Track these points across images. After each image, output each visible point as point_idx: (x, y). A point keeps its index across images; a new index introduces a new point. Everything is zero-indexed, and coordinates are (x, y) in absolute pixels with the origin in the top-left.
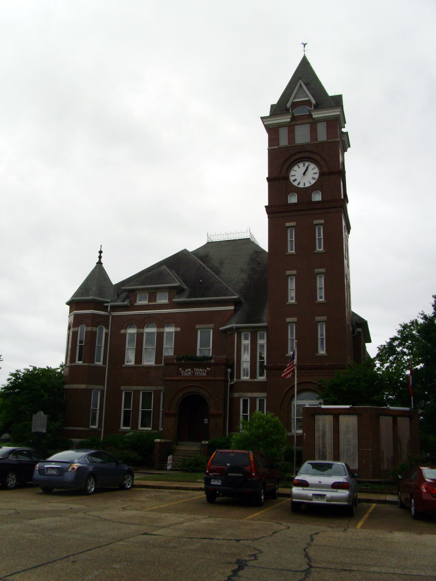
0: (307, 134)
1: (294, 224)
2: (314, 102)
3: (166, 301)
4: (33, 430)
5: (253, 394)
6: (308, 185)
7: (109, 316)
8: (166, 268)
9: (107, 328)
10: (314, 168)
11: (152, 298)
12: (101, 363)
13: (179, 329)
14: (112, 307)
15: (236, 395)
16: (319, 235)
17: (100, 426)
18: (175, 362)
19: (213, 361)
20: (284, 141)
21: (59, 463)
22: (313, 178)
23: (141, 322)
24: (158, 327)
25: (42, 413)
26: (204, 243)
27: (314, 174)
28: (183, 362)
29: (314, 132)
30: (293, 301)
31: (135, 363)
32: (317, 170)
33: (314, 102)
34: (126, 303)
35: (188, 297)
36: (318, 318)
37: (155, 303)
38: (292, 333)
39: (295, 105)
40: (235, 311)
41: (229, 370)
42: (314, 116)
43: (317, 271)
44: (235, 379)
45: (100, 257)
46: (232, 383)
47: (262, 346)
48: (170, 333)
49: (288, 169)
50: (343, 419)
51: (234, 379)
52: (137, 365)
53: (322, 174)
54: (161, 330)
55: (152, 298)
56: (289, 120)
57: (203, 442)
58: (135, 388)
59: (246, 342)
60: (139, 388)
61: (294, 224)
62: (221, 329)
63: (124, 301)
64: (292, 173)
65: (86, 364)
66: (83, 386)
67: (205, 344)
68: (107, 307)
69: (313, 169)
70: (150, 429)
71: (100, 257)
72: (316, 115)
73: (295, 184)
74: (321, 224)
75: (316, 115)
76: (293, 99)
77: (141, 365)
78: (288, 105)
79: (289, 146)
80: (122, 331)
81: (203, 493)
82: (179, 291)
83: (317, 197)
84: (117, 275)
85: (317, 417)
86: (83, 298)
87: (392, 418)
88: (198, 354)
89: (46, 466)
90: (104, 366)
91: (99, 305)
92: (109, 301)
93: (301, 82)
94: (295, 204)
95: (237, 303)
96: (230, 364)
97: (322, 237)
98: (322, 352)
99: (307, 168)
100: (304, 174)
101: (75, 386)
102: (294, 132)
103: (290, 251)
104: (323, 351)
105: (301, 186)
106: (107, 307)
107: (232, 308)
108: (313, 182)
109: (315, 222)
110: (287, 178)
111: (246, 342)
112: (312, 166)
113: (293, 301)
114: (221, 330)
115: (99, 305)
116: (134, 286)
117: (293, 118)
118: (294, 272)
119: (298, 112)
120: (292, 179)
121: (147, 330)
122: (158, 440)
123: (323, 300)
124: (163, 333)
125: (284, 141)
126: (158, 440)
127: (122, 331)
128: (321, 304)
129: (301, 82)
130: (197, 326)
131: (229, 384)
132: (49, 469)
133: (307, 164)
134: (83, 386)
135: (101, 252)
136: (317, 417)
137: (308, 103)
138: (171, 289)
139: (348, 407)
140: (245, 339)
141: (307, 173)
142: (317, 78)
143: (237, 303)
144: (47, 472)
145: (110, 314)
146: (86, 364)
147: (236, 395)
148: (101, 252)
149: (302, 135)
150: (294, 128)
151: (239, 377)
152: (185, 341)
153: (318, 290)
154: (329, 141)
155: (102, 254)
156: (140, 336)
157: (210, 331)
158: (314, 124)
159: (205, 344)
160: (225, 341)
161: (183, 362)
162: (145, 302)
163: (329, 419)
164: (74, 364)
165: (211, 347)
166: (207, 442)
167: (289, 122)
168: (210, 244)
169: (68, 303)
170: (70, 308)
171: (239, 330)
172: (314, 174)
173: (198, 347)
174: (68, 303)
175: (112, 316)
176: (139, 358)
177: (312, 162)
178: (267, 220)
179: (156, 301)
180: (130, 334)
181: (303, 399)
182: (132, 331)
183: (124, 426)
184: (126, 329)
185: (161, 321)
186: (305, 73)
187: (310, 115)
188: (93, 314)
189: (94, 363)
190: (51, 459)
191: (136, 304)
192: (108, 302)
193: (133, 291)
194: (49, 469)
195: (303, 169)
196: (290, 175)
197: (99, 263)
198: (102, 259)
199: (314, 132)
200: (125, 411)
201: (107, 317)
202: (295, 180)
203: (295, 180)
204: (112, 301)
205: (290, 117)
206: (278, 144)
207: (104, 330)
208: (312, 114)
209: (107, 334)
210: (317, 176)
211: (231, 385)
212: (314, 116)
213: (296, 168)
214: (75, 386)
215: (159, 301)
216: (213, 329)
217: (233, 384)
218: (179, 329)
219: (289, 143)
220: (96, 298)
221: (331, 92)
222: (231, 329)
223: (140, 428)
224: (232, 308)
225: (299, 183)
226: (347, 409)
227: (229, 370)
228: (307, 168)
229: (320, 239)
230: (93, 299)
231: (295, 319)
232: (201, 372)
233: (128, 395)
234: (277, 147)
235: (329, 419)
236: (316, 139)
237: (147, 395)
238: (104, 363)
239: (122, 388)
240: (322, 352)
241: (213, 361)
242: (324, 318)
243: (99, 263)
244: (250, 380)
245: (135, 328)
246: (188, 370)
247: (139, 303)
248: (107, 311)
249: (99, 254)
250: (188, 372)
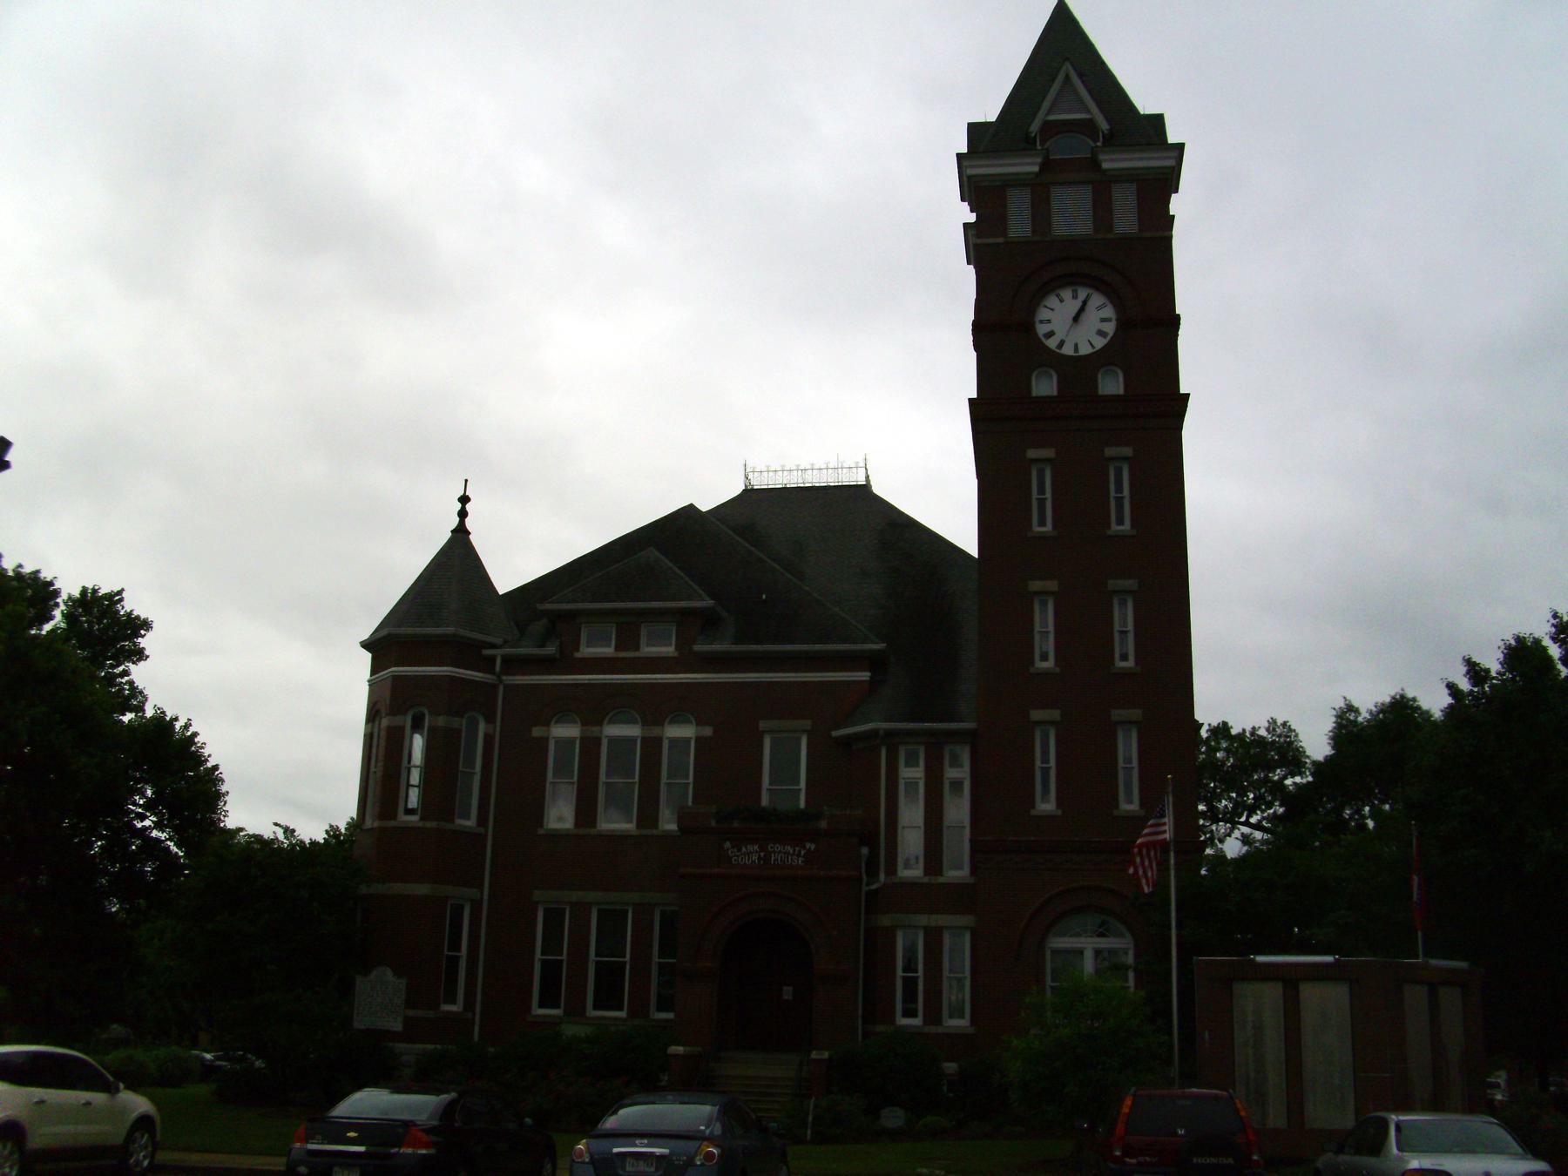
0: (1069, 208)
1: (1049, 453)
2: (1104, 126)
3: (669, 650)
4: (358, 1024)
5: (934, 917)
6: (1085, 350)
7: (494, 687)
8: (657, 554)
9: (490, 720)
11: (628, 639)
12: (470, 823)
13: (708, 731)
14: (506, 660)
15: (885, 921)
16: (1119, 489)
17: (469, 1005)
18: (713, 824)
19: (823, 824)
20: (1019, 226)
21: (661, 1141)
22: (1101, 333)
23: (595, 707)
24: (645, 723)
25: (389, 972)
26: (736, 489)
27: (1103, 320)
28: (736, 824)
29: (1102, 209)
30: (1049, 664)
31: (577, 824)
32: (1109, 312)
33: (1104, 126)
34: (551, 650)
35: (737, 641)
36: (1117, 714)
37: (636, 654)
38: (1045, 752)
39: (1050, 129)
40: (873, 684)
41: (865, 851)
42: (1105, 166)
43: (1113, 584)
44: (882, 877)
45: (463, 514)
46: (874, 887)
47: (957, 785)
48: (567, 743)
50: (1311, 994)
51: (877, 875)
52: (583, 831)
53: (1124, 324)
54: (656, 731)
55: (628, 639)
56: (1036, 169)
57: (814, 1055)
58: (575, 896)
59: (912, 774)
60: (591, 896)
61: (1049, 453)
62: (834, 734)
63: (543, 646)
64: (1043, 314)
65: (429, 824)
66: (422, 889)
67: (786, 772)
68: (493, 659)
69: (1099, 308)
70: (623, 1014)
71: (463, 514)
72: (1110, 162)
73: (1052, 343)
74: (1125, 459)
76: (1049, 112)
77: (593, 831)
78: (1035, 127)
79: (1036, 238)
80: (537, 732)
82: (708, 623)
83: (1111, 385)
84: (512, 565)
85: (1238, 987)
86: (419, 630)
87: (1280, 985)
88: (765, 801)
89: (615, 1150)
90: (481, 830)
91: (466, 651)
92: (499, 641)
95: (875, 663)
96: (875, 837)
97: (1048, 495)
98: (1047, 806)
99: (1085, 303)
100: (1076, 319)
101: (397, 888)
102: (1047, 201)
103: (1115, 528)
104: (1130, 802)
105: (1068, 350)
106: (493, 659)
107: (865, 676)
108: (1100, 343)
109: (1110, 452)
110: (1028, 327)
111: (912, 774)
112: (1097, 299)
113: (1130, 664)
114: (837, 738)
115: (466, 651)
116: (574, 601)
117: (1046, 165)
118: (1053, 585)
120: (1041, 330)
121: (674, 731)
122: (680, 1049)
123: (1130, 664)
124: (659, 740)
125: (1019, 226)
126: (680, 1049)
127: (537, 732)
128: (1126, 675)
130: (763, 725)
131: (865, 889)
132: (629, 1160)
133: (1083, 293)
134: (422, 889)
135: (464, 500)
136: (1238, 987)
137: (1088, 127)
138: (683, 616)
139: (1329, 959)
140: (908, 765)
141: (1083, 317)
142: (1103, 63)
143: (875, 663)
144: (624, 1168)
145: (501, 681)
146: (429, 824)
147: (885, 921)
148: (464, 500)
149: (1072, 214)
151: (891, 870)
152: (727, 762)
153: (1117, 636)
154: (1148, 235)
155: (468, 507)
156: (590, 746)
157: (799, 739)
158: (1103, 185)
159: (786, 772)
160: (851, 770)
161: (736, 824)
162: (608, 651)
163: (1271, 993)
164: (392, 823)
165: (637, 779)
166: (826, 1055)
167: (1037, 175)
168: (750, 496)
169: (366, 645)
170: (373, 659)
171: (892, 740)
172: (1103, 320)
173: (603, 778)
174: (366, 645)
175: (506, 686)
176: (586, 811)
177: (1097, 289)
178: (1184, 433)
179: (637, 648)
180: (558, 741)
181: (1078, 935)
182: (566, 731)
183: (542, 1005)
184: (547, 724)
185: (655, 706)
186: (1064, 50)
187: (1094, 163)
188: (452, 679)
189: (452, 821)
190: (611, 1122)
191: (578, 655)
192: (493, 646)
193: (572, 616)
194: (629, 1160)
195: (1072, 306)
196: (1037, 320)
197: (461, 532)
198: (467, 521)
199: (1102, 209)
200: (544, 963)
201: (494, 687)
202: (1050, 334)
203: (1050, 334)
204: (506, 642)
205: (1039, 160)
206: (1005, 234)
207: (482, 726)
208: (1101, 157)
209: (489, 740)
210: (1110, 328)
211: (868, 893)
212: (1105, 166)
213: (1052, 301)
214: (397, 888)
215: (649, 650)
216: (810, 734)
217: (877, 891)
218: (708, 731)
219: (1034, 232)
220: (462, 632)
221: (1145, 105)
222: (873, 734)
223: (592, 1013)
224: (865, 676)
226: (1327, 965)
227: (865, 851)
228: (1085, 303)
229: (1119, 500)
230: (454, 635)
231: (1055, 714)
232: (788, 855)
233: (554, 918)
234: (1001, 240)
235: (1271, 993)
236: (1110, 228)
237: (612, 920)
238: (482, 820)
239: (538, 895)
240: (1047, 806)
241: (823, 824)
242: (1135, 714)
243: (461, 532)
244: (926, 880)
245: (574, 722)
246: (750, 848)
247: (587, 651)
248: (493, 673)
250: (749, 855)
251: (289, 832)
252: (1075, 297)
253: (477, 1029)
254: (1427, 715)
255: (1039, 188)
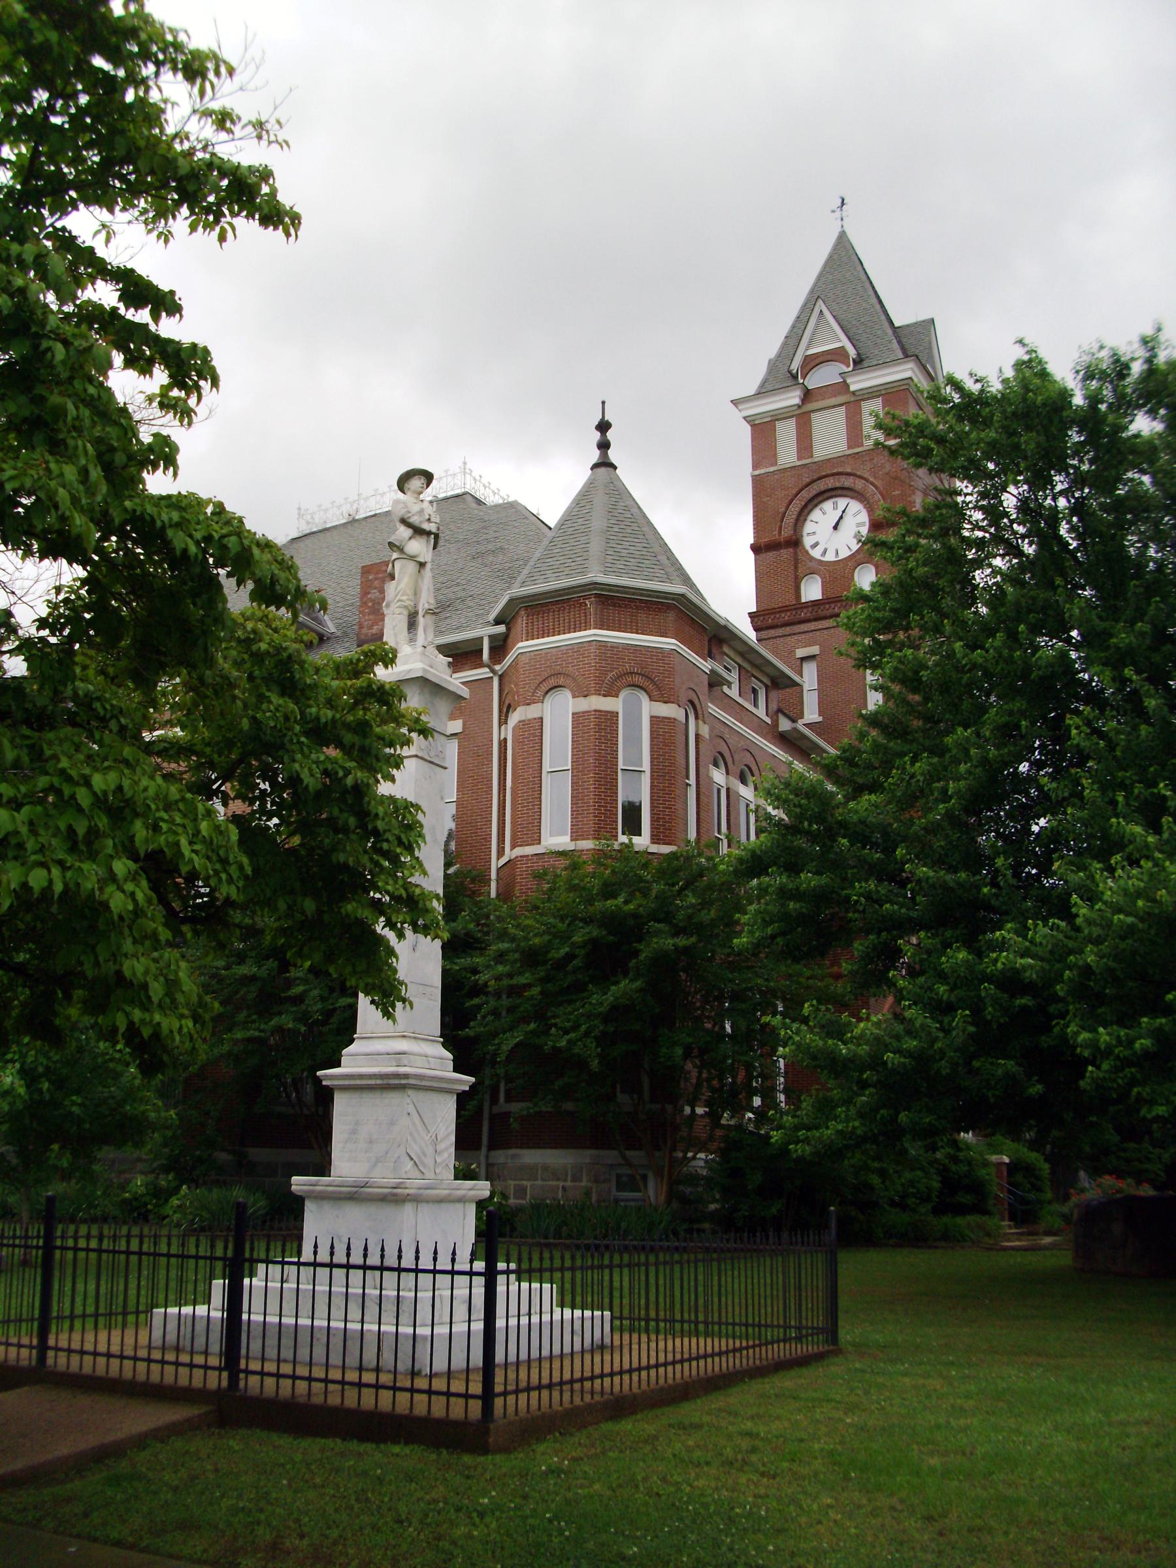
1: (815, 650)
2: (852, 352)
6: (844, 554)
10: (859, 512)
20: (787, 454)
27: (825, 551)
33: (852, 352)
39: (812, 362)
45: (604, 446)
49: (797, 520)
56: (797, 401)
64: (809, 527)
69: (855, 515)
71: (604, 446)
72: (859, 382)
75: (859, 382)
78: (795, 366)
81: (201, 1385)
93: (820, 305)
94: (815, 603)
100: (835, 528)
105: (830, 557)
110: (795, 542)
112: (855, 506)
117: (807, 395)
119: (819, 378)
120: (808, 542)
125: (787, 454)
129: (820, 305)
133: (842, 502)
135: (603, 426)
137: (838, 355)
141: (842, 523)
148: (603, 426)
150: (810, 420)
186: (843, 279)
213: (816, 515)
225: (825, 551)
249: (597, 435)
251: (388, 606)
252: (835, 508)
253: (493, 885)
254: (23, 677)
255: (803, 419)
